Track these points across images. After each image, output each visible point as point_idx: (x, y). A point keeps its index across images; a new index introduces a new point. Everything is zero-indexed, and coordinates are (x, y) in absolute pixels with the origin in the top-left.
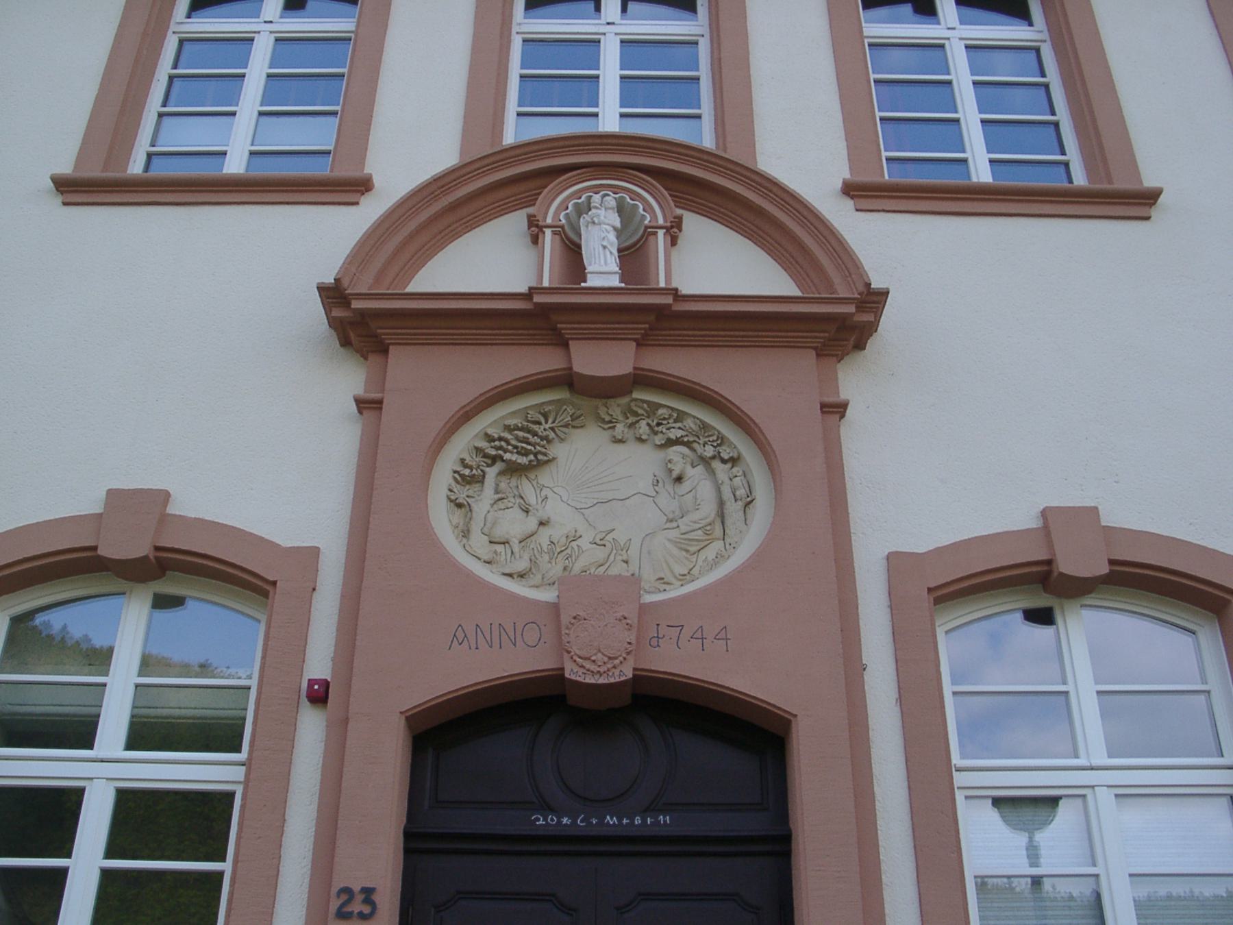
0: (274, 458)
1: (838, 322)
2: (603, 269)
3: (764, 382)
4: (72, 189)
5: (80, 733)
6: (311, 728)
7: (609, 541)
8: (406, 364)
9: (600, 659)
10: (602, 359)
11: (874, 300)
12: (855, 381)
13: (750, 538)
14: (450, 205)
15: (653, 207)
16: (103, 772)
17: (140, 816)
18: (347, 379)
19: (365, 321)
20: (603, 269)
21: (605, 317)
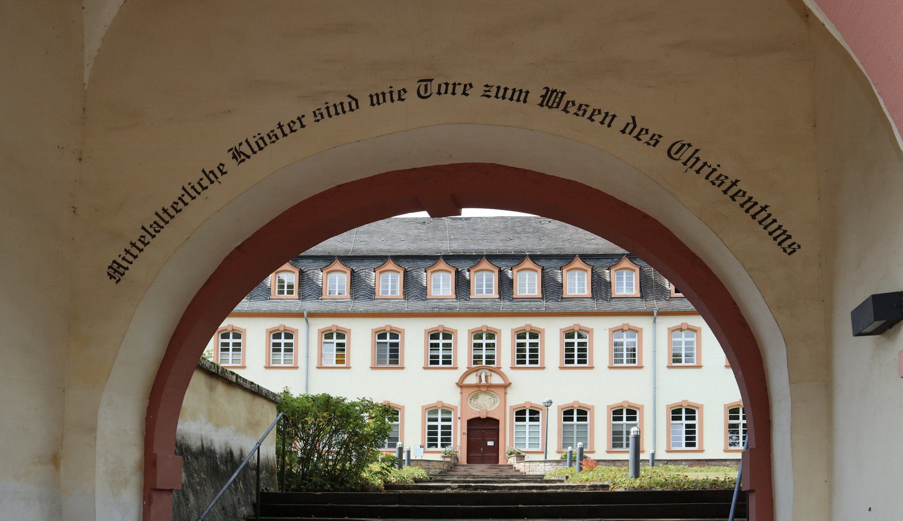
0: (452, 398)
1: (506, 386)
2: (484, 382)
3: (501, 391)
4: (318, 368)
5: (285, 344)
6: (459, 421)
7: (485, 406)
8: (464, 389)
9: (483, 416)
10: (482, 389)
11: (510, 384)
12: (509, 390)
13: (497, 405)
14: (466, 375)
15: (488, 373)
16: (440, 424)
17: (443, 427)
18: (459, 390)
19: (461, 385)
20: (484, 382)
21: (484, 386)
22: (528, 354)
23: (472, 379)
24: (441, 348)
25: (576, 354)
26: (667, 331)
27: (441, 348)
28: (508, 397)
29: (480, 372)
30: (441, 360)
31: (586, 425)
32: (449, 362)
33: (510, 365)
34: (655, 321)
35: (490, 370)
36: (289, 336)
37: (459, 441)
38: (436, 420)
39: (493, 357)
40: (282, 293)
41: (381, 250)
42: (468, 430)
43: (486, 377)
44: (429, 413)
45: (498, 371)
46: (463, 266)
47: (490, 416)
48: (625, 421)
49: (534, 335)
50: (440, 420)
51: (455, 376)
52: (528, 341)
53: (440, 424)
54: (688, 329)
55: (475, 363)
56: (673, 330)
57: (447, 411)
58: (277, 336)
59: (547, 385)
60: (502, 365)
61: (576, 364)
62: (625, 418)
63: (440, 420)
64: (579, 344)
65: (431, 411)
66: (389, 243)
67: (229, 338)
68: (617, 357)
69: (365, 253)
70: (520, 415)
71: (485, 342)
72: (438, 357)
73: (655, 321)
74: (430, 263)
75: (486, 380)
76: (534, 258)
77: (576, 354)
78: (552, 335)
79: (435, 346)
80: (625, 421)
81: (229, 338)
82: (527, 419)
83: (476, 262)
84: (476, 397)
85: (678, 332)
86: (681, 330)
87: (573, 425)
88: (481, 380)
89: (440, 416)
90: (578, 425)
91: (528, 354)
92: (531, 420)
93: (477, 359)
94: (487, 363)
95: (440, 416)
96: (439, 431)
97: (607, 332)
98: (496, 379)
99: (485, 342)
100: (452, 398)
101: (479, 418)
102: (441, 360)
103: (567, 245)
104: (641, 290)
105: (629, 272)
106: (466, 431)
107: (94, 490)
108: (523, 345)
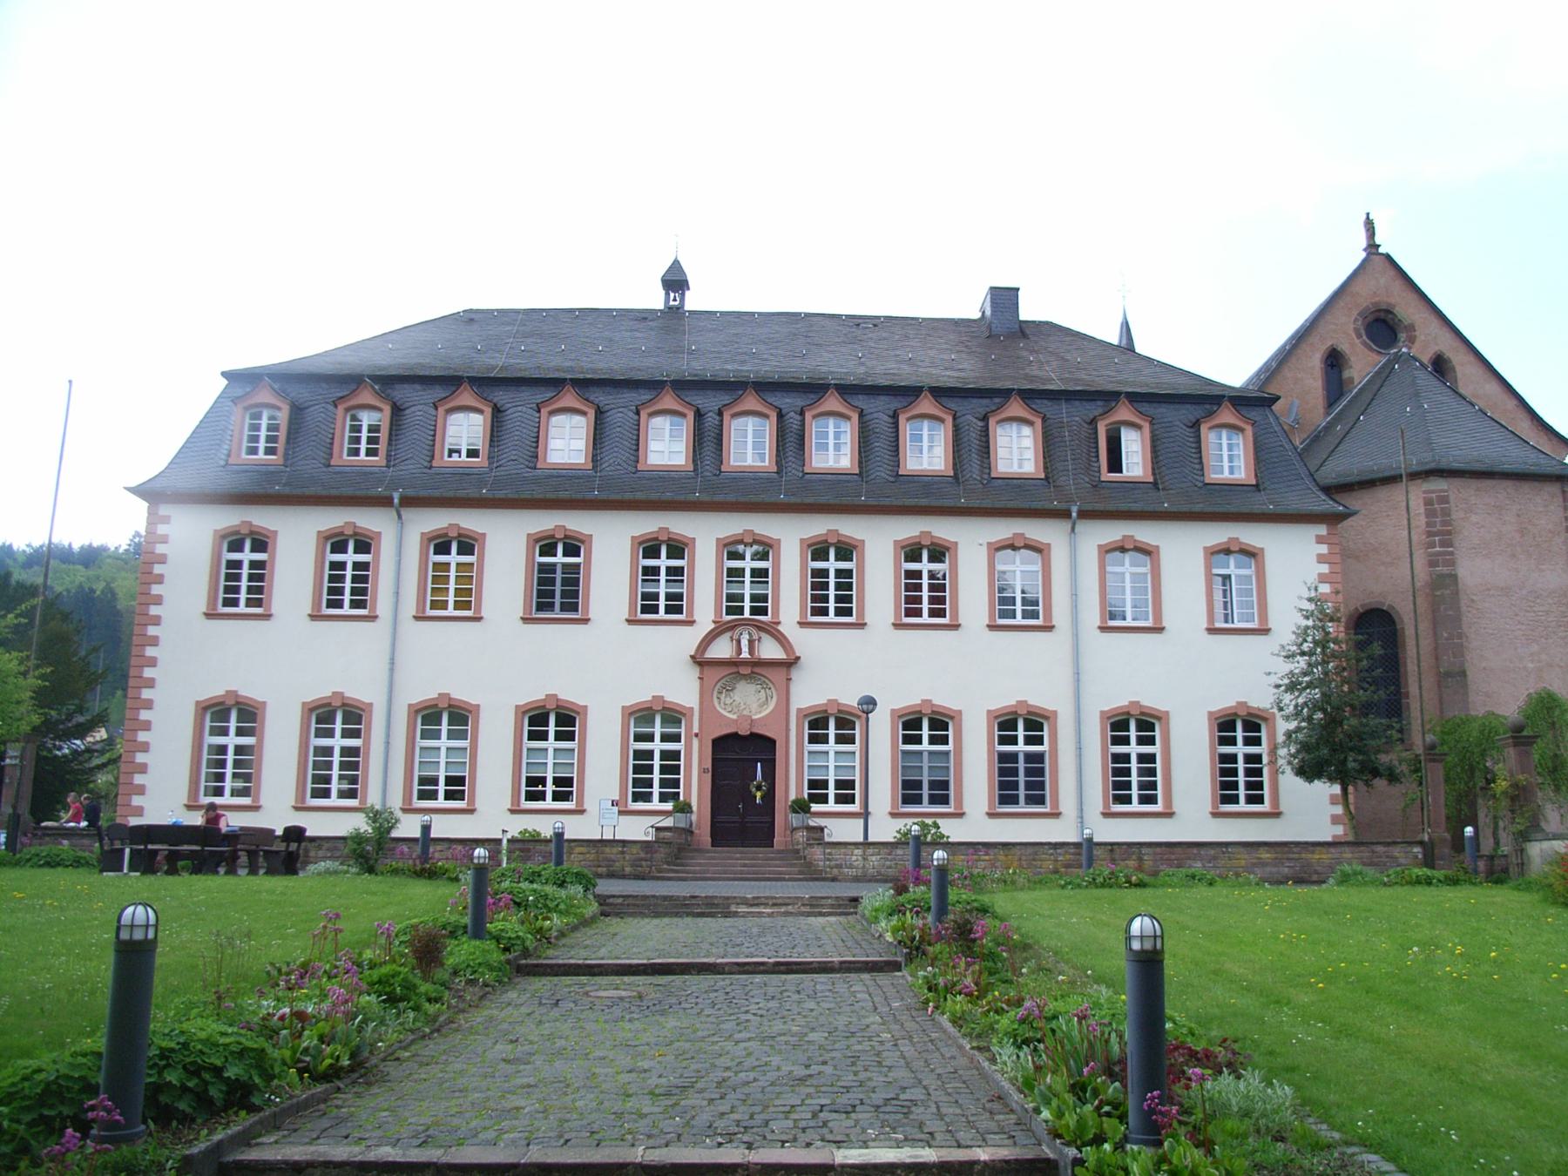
0: (684, 690)
1: (791, 663)
2: (745, 655)
3: (777, 675)
4: (417, 618)
5: (668, 569)
7: (748, 706)
8: (706, 669)
9: (744, 732)
10: (745, 671)
12: (795, 674)
16: (657, 746)
19: (700, 661)
21: (745, 663)
22: (833, 598)
23: (722, 649)
24: (663, 576)
25: (925, 600)
26: (1202, 554)
27: (663, 576)
28: (795, 689)
29: (737, 631)
30: (662, 603)
31: (947, 753)
32: (679, 610)
33: (1098, 623)
34: (1073, 529)
35: (760, 628)
36: (363, 546)
37: (695, 785)
38: (650, 738)
39: (679, 597)
40: (356, 452)
41: (594, 371)
42: (714, 760)
43: (751, 642)
44: (638, 723)
45: (773, 631)
46: (710, 402)
47: (756, 730)
48: (925, 746)
49: (260, 545)
50: (657, 737)
51: (688, 639)
52: (832, 565)
53: (657, 746)
54: (1027, 547)
55: (730, 611)
56: (997, 548)
57: (673, 715)
58: (652, 551)
59: (863, 663)
60: (782, 618)
61: (832, 617)
62: (925, 739)
63: (657, 737)
64: (839, 573)
65: (642, 715)
66: (573, 356)
67: (345, 552)
68: (1003, 604)
69: (526, 374)
70: (817, 724)
71: (748, 564)
72: (656, 597)
73: (1073, 529)
74: (645, 396)
75: (751, 651)
76: (847, 390)
77: (925, 600)
78: (506, 542)
79: (651, 572)
80: (925, 746)
81: (345, 552)
82: (832, 738)
83: (910, 399)
84: (729, 689)
85: (1117, 553)
86: (1123, 550)
87: (920, 753)
88: (739, 651)
89: (658, 730)
90: (931, 753)
91: (833, 598)
92: (841, 739)
93: (733, 604)
94: (754, 611)
95: (658, 730)
96: (336, 759)
97: (984, 551)
98: (770, 650)
99: (748, 564)
100: (684, 690)
101: (735, 736)
102: (662, 603)
103: (1083, 375)
104: (860, 463)
105: (756, 420)
106: (709, 765)
107: (665, 898)
108: (824, 573)
